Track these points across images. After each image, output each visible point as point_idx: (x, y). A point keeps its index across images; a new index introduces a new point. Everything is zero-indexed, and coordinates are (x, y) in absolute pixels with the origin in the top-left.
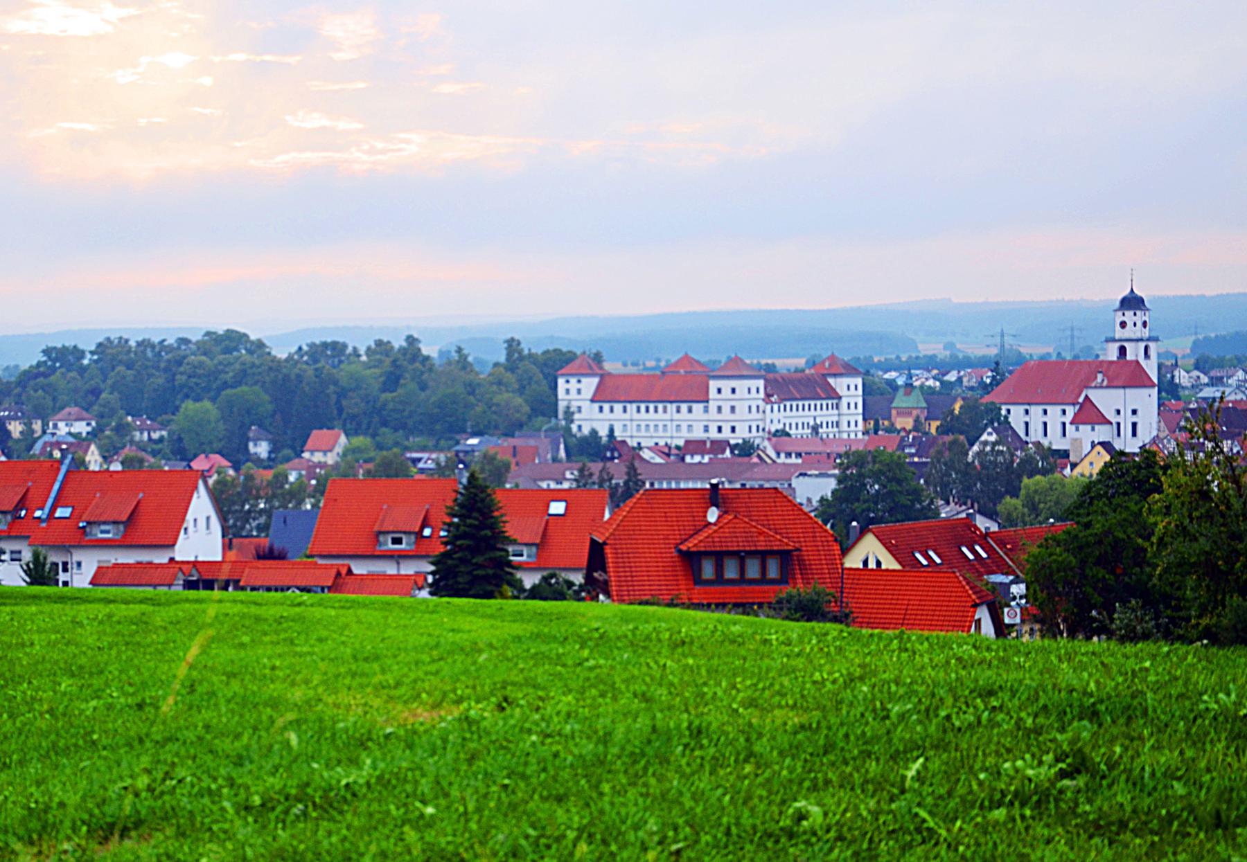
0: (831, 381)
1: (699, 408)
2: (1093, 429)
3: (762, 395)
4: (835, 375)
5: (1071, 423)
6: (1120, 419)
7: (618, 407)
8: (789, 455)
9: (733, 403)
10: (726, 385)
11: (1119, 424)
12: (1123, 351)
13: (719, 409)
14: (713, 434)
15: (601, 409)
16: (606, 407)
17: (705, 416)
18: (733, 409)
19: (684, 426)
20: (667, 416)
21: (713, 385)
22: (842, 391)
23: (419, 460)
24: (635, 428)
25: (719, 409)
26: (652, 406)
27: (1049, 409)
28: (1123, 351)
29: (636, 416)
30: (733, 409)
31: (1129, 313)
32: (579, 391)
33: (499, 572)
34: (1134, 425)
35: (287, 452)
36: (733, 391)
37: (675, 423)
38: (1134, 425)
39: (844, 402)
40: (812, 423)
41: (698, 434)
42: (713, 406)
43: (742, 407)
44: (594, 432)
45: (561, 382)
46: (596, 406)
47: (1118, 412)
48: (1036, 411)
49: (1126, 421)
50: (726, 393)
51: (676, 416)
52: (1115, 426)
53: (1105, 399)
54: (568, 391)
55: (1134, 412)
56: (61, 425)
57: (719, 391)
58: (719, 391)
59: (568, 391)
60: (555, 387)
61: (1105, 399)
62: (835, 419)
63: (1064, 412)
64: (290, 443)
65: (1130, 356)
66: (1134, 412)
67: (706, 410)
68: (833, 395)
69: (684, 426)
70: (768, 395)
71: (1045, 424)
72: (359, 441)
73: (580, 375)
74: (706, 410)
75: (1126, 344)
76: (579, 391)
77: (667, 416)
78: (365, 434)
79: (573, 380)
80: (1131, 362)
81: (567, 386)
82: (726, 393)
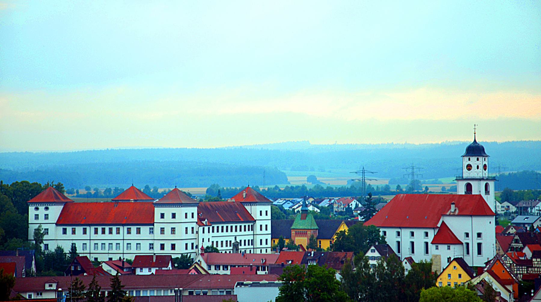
1: (145, 230)
2: (449, 249)
3: (196, 219)
9: (173, 226)
10: (168, 211)
11: (468, 244)
12: (469, 187)
13: (162, 230)
16: (69, 229)
17: (151, 237)
18: (173, 230)
19: (134, 244)
20: (87, 237)
24: (125, 245)
25: (162, 230)
28: (469, 187)
29: (94, 236)
30: (173, 230)
34: (479, 245)
36: (174, 216)
37: (126, 242)
38: (479, 245)
39: (258, 224)
40: (233, 241)
46: (61, 228)
47: (467, 235)
48: (406, 233)
50: (168, 217)
52: (465, 245)
55: (479, 235)
57: (162, 216)
58: (162, 216)
62: (251, 238)
63: (427, 234)
65: (475, 192)
66: (479, 235)
69: (134, 244)
71: (413, 243)
77: (120, 236)
81: (37, 212)
82: (168, 217)
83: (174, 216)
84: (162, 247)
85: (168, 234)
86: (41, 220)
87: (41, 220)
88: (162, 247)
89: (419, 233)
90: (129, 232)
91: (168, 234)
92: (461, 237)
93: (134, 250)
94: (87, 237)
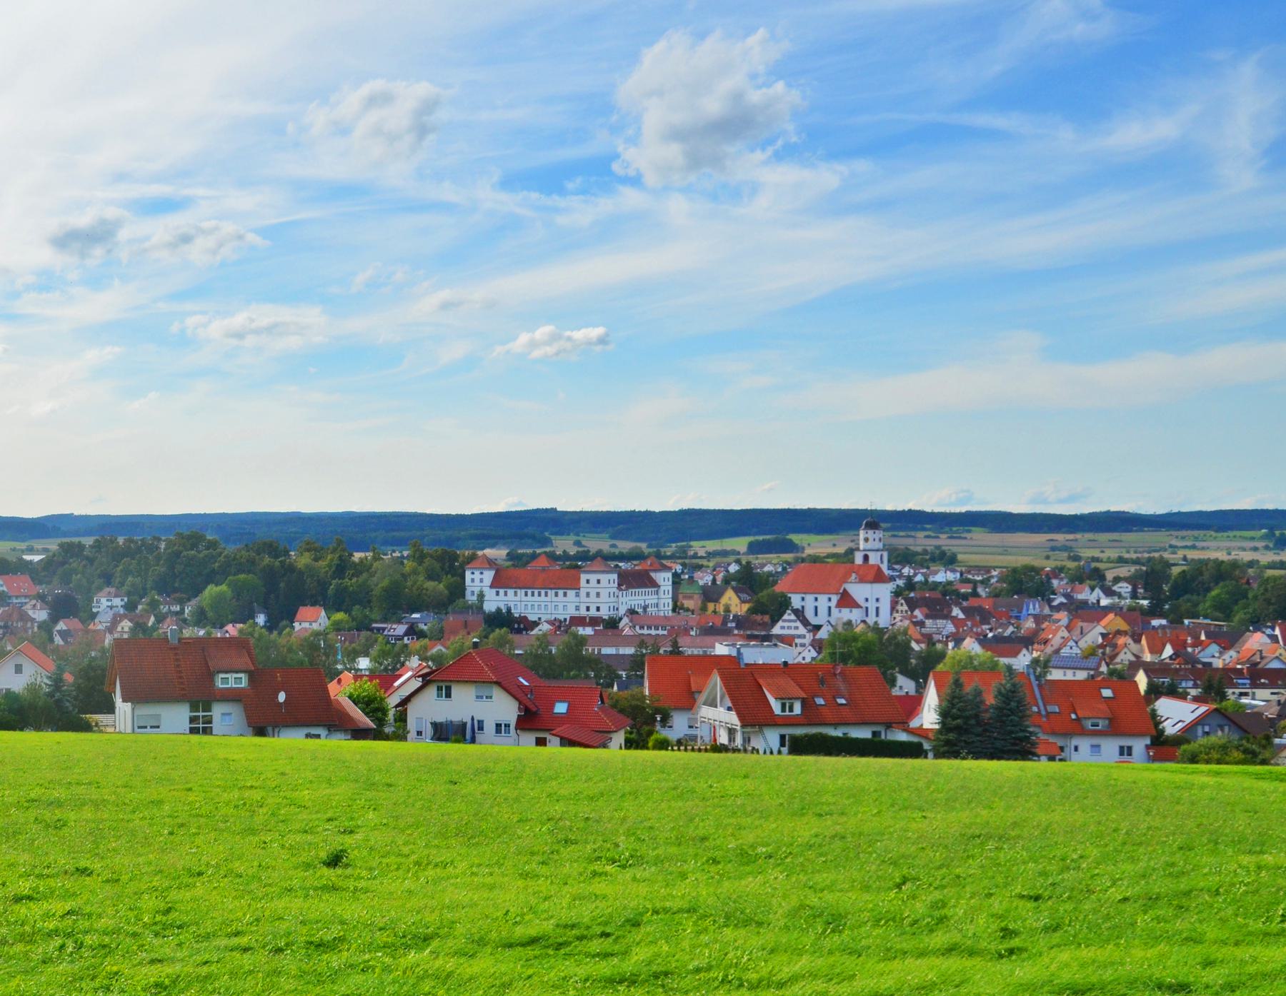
0: (653, 575)
1: (571, 593)
4: (655, 571)
5: (492, 586)
6: (868, 605)
7: (511, 592)
8: (641, 628)
10: (593, 578)
12: (866, 558)
13: (588, 595)
14: (593, 612)
15: (498, 593)
17: (577, 599)
18: (598, 595)
21: (584, 577)
22: (660, 582)
23: (384, 629)
25: (588, 595)
26: (536, 592)
27: (820, 597)
29: (524, 598)
30: (598, 595)
31: (870, 532)
32: (481, 581)
33: (125, 588)
34: (877, 609)
35: (646, 728)
36: (599, 582)
38: (877, 609)
41: (583, 612)
42: (583, 592)
43: (604, 593)
44: (499, 610)
45: (468, 575)
46: (494, 591)
48: (810, 598)
49: (872, 606)
50: (593, 583)
51: (555, 599)
53: (858, 591)
54: (473, 580)
55: (877, 600)
56: (103, 600)
57: (588, 581)
58: (588, 581)
59: (473, 580)
60: (463, 578)
61: (858, 591)
64: (282, 615)
66: (877, 600)
67: (577, 595)
68: (654, 584)
70: (619, 585)
72: (340, 616)
73: (482, 569)
74: (577, 595)
75: (870, 554)
76: (481, 581)
78: (346, 612)
79: (477, 573)
80: (873, 566)
82: (593, 583)
83: (599, 582)
84: (588, 609)
85: (593, 597)
86: (477, 582)
87: (477, 582)
88: (588, 609)
89: (823, 599)
90: (556, 595)
91: (593, 597)
92: (861, 601)
93: (561, 610)
94: (518, 598)
